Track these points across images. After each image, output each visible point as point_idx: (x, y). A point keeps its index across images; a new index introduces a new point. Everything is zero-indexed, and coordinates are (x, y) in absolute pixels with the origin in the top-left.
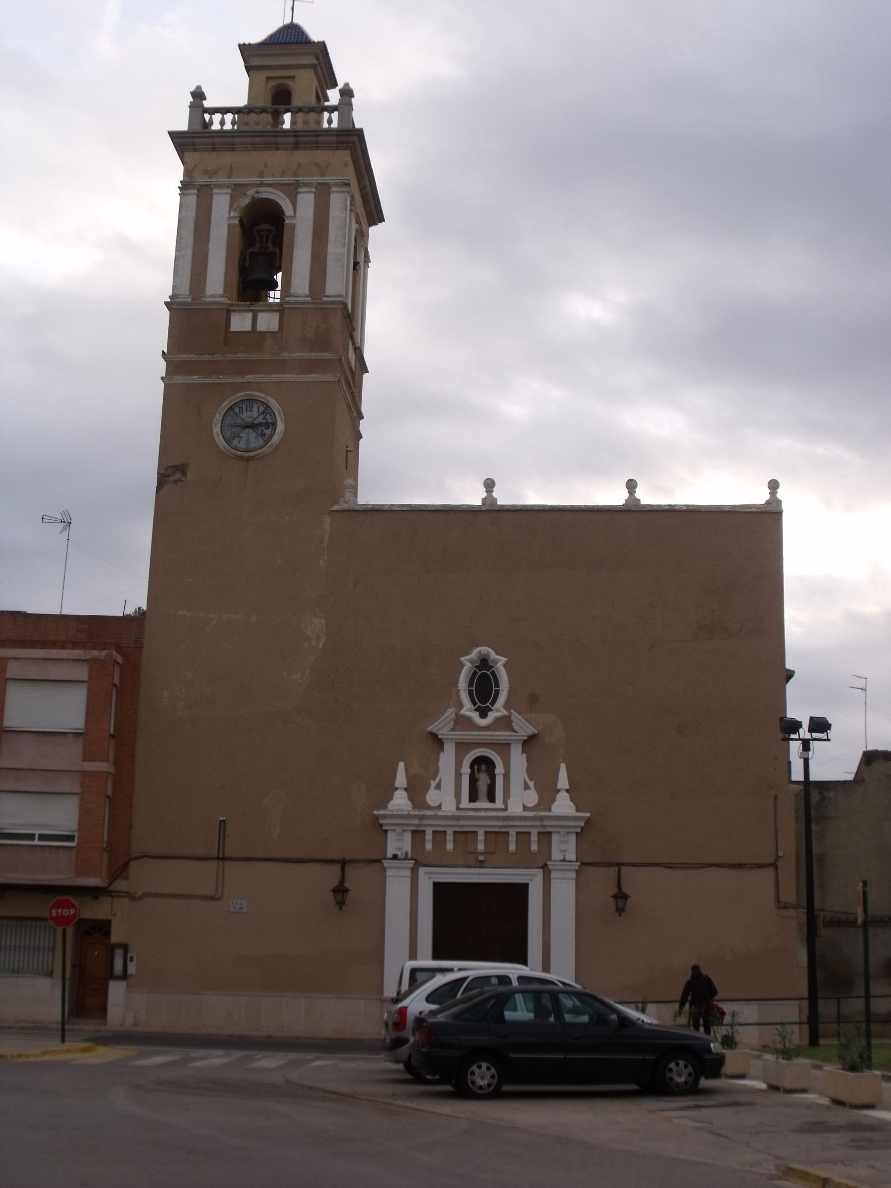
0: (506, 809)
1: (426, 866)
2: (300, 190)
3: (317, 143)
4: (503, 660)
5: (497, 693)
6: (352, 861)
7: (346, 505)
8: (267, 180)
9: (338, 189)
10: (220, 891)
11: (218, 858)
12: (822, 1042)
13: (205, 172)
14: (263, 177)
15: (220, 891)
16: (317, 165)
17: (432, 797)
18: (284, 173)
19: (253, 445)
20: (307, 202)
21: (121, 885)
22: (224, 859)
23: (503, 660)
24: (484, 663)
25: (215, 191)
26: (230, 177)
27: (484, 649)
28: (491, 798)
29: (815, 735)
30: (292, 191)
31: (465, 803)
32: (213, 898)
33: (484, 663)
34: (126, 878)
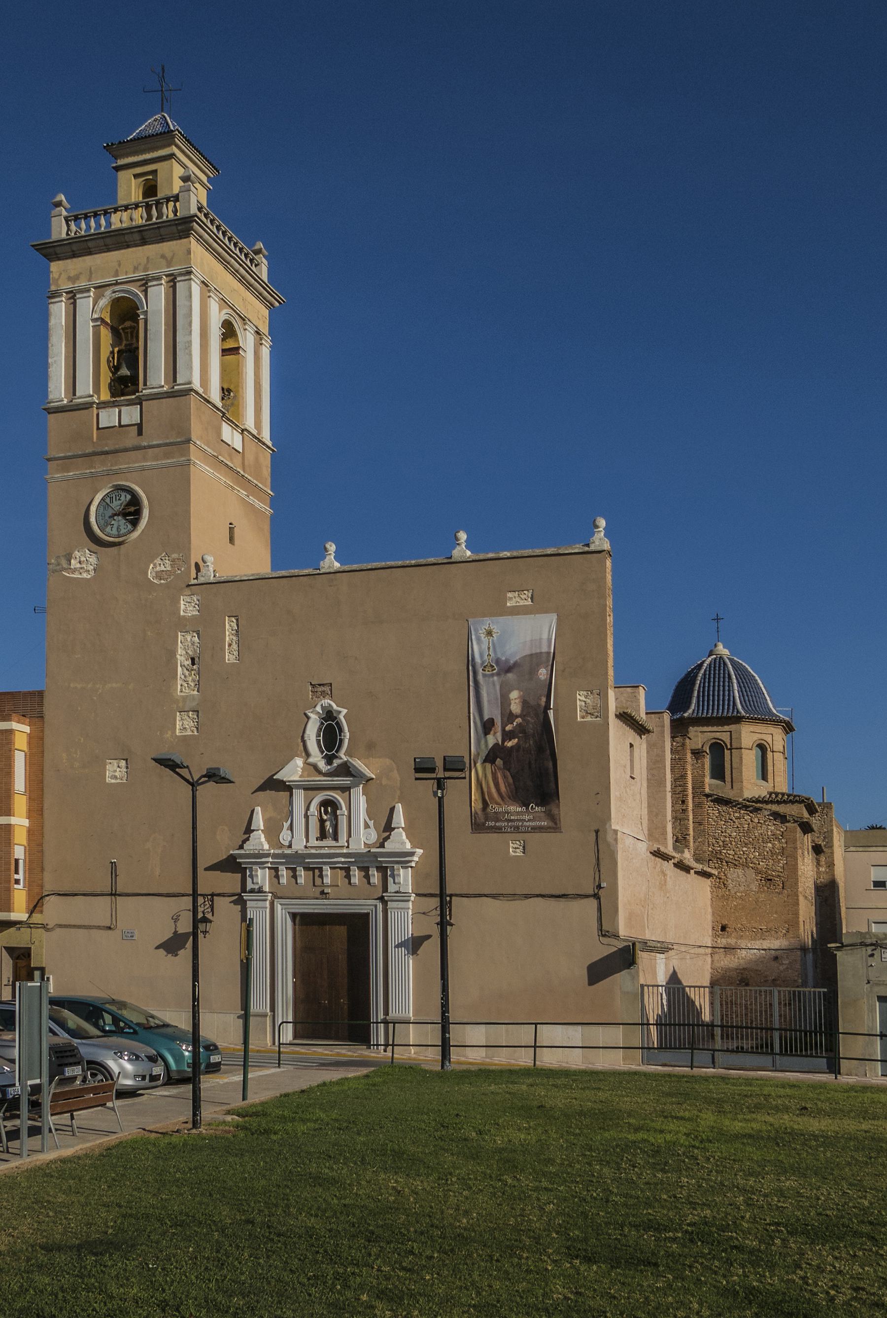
0: (348, 847)
1: (281, 898)
2: (150, 284)
3: (56, 254)
4: (344, 711)
5: (341, 741)
6: (219, 895)
7: (203, 579)
8: (122, 277)
9: (183, 278)
10: (114, 922)
11: (111, 894)
12: (844, 1064)
13: (69, 278)
14: (118, 276)
15: (114, 922)
16: (163, 256)
17: (285, 836)
18: (136, 269)
19: (123, 531)
20: (158, 295)
21: (37, 918)
22: (115, 895)
23: (344, 711)
24: (329, 715)
25: (178, 279)
26: (90, 280)
27: (326, 702)
28: (336, 838)
29: (448, 774)
30: (145, 283)
31: (313, 842)
32: (110, 928)
33: (329, 715)
34: (41, 912)
